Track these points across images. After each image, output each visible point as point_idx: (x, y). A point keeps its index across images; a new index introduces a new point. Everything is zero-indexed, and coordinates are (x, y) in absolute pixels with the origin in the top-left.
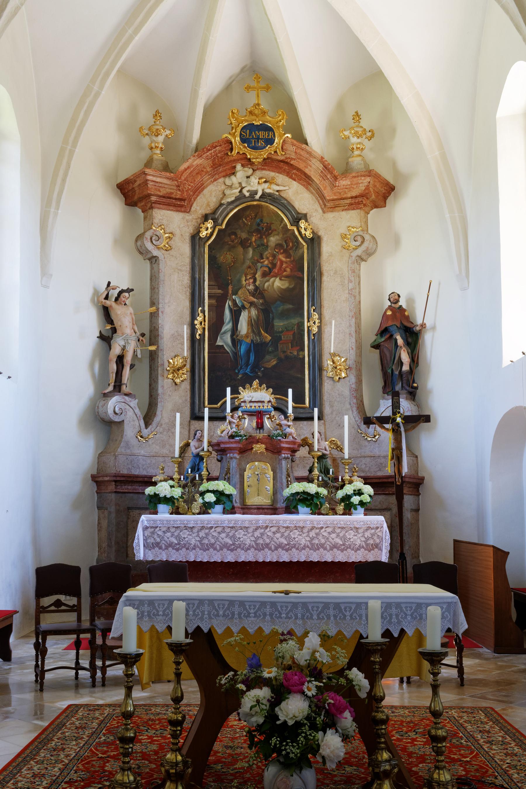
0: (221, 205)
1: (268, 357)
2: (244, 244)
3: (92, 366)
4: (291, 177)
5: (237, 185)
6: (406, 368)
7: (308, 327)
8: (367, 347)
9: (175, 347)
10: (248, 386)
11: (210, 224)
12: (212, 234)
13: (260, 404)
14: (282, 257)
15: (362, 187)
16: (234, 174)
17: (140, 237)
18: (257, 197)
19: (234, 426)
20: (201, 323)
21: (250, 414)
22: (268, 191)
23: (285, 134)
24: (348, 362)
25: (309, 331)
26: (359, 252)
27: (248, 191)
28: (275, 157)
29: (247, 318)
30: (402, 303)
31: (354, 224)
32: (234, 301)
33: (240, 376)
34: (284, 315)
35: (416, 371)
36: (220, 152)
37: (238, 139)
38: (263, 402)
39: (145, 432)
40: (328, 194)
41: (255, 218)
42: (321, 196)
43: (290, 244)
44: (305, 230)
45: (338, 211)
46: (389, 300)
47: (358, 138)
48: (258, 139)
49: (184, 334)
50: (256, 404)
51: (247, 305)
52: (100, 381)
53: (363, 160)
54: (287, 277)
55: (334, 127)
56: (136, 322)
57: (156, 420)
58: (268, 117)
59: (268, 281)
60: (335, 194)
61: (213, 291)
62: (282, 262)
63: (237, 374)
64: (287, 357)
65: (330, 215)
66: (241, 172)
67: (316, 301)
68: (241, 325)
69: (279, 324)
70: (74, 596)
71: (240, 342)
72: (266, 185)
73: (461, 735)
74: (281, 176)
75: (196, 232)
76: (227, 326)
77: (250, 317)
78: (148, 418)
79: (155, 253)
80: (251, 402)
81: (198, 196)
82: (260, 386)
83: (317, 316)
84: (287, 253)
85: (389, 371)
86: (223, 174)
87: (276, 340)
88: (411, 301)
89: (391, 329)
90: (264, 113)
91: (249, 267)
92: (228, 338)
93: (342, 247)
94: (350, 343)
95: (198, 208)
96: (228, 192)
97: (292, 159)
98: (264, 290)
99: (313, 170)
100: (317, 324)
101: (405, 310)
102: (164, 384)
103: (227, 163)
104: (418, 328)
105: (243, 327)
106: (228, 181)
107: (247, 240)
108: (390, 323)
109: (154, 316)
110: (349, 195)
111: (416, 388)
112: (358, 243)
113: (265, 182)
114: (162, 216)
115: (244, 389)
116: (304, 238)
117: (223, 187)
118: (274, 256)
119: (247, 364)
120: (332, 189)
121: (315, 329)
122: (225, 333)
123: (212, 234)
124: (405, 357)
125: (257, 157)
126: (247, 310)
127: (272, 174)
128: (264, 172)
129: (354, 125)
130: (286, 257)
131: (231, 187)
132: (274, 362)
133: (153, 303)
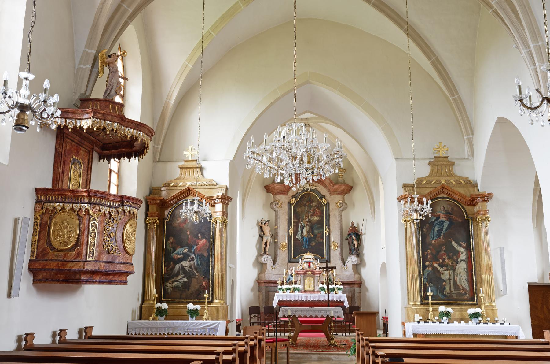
2: (305, 205)
3: (256, 246)
6: (356, 246)
8: (344, 239)
9: (283, 239)
17: (272, 204)
21: (307, 262)
26: (341, 209)
30: (355, 225)
34: (318, 228)
35: (360, 248)
39: (274, 267)
43: (320, 205)
49: (309, 326)
52: (259, 251)
56: (271, 231)
57: (277, 263)
65: (332, 196)
69: (316, 231)
76: (300, 232)
78: (274, 262)
79: (277, 209)
88: (358, 224)
92: (300, 236)
102: (279, 252)
105: (305, 232)
109: (276, 229)
114: (278, 197)
116: (324, 204)
121: (327, 234)
124: (356, 243)
133: (276, 225)
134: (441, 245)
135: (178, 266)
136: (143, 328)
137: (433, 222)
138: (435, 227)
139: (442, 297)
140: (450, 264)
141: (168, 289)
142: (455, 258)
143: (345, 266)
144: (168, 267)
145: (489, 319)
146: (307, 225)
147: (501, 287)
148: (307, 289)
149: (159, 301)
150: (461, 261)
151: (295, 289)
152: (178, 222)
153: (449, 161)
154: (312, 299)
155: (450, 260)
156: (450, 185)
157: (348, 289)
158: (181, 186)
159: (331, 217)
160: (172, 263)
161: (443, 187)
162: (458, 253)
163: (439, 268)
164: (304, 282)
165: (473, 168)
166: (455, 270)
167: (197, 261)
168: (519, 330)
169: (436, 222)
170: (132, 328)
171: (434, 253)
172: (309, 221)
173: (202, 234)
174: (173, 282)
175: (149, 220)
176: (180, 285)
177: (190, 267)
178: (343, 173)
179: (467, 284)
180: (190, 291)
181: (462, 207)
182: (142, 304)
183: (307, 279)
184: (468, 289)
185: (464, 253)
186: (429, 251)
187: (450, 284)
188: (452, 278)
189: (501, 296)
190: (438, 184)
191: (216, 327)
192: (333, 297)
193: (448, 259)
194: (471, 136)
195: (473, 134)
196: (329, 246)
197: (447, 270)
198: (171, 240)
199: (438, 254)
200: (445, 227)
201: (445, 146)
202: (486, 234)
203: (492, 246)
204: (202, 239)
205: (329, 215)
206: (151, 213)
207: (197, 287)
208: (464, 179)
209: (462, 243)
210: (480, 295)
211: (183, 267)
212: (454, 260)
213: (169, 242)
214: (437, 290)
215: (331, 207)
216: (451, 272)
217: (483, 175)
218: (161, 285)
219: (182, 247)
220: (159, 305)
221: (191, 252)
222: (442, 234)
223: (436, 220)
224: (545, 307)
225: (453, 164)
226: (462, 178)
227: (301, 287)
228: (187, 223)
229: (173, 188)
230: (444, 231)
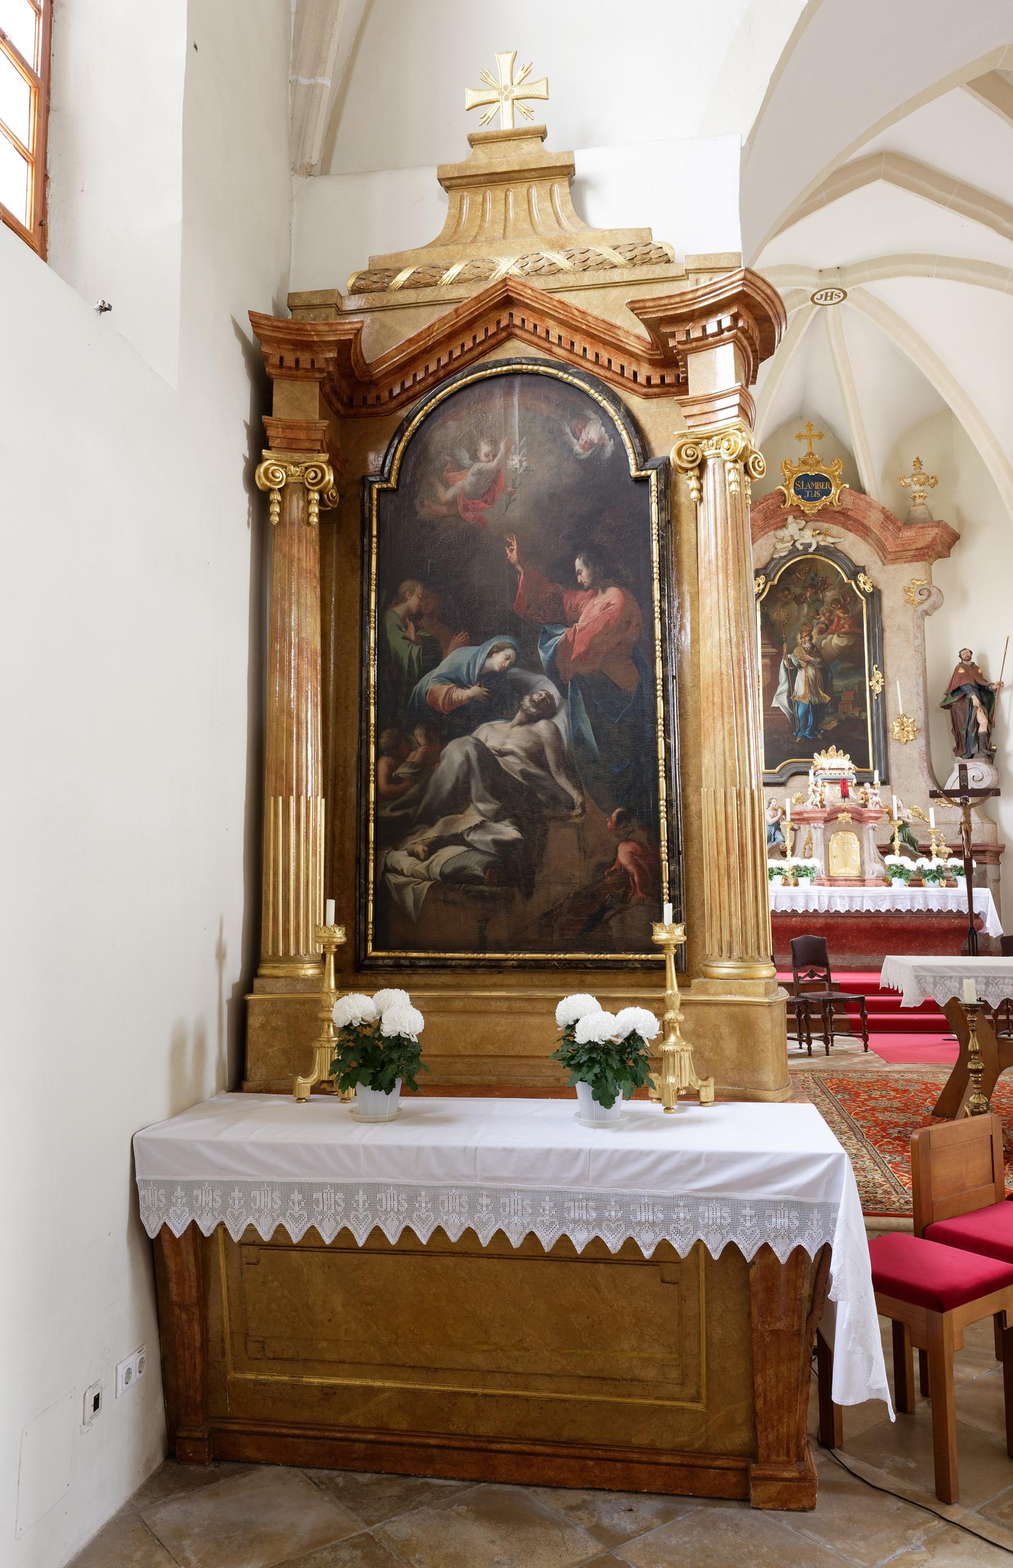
0: (772, 559)
1: (827, 719)
2: (799, 600)
4: (847, 528)
5: (789, 538)
6: (983, 729)
12: (764, 590)
15: (929, 538)
18: (811, 550)
21: (833, 781)
22: (822, 543)
24: (916, 724)
25: (871, 691)
26: (925, 606)
27: (802, 544)
29: (803, 678)
32: (789, 661)
34: (844, 674)
35: (994, 732)
36: (772, 504)
37: (792, 491)
40: (890, 545)
43: (848, 599)
44: (865, 583)
46: (960, 656)
48: (814, 489)
51: (803, 664)
53: (927, 509)
54: (845, 633)
55: (890, 474)
60: (897, 546)
61: (767, 650)
62: (839, 618)
63: (795, 737)
65: (891, 568)
66: (793, 527)
67: (879, 660)
69: (838, 684)
72: (820, 538)
73: (890, 1166)
76: (783, 687)
83: (881, 675)
84: (844, 608)
85: (964, 732)
87: (836, 701)
88: (982, 657)
89: (965, 688)
91: (805, 624)
93: (906, 601)
94: (918, 703)
96: (779, 546)
99: (873, 520)
101: (978, 668)
104: (994, 687)
106: (781, 533)
107: (801, 595)
108: (964, 682)
111: (995, 751)
112: (924, 597)
113: (819, 534)
116: (863, 592)
117: (774, 540)
118: (831, 612)
119: (806, 728)
120: (894, 540)
121: (878, 689)
122: (780, 694)
124: (982, 719)
127: (826, 525)
128: (817, 523)
129: (914, 472)
131: (782, 540)
135: (455, 754)
136: (247, 1187)
141: (400, 888)
144: (399, 759)
148: (836, 871)
149: (356, 971)
151: (800, 872)
152: (447, 495)
154: (868, 906)
158: (458, 281)
160: (419, 735)
164: (827, 848)
167: (573, 717)
170: (170, 1186)
172: (814, 650)
173: (596, 557)
174: (434, 847)
175: (276, 469)
176: (475, 864)
177: (535, 754)
178: (928, 489)
180: (539, 903)
182: (248, 983)
191: (811, 1187)
198: (413, 602)
204: (597, 586)
206: (289, 426)
207: (581, 875)
211: (488, 759)
213: (399, 610)
215: (888, 603)
218: (361, 864)
219: (476, 639)
220: (354, 1007)
221: (535, 666)
227: (815, 862)
228: (501, 498)
229: (411, 296)
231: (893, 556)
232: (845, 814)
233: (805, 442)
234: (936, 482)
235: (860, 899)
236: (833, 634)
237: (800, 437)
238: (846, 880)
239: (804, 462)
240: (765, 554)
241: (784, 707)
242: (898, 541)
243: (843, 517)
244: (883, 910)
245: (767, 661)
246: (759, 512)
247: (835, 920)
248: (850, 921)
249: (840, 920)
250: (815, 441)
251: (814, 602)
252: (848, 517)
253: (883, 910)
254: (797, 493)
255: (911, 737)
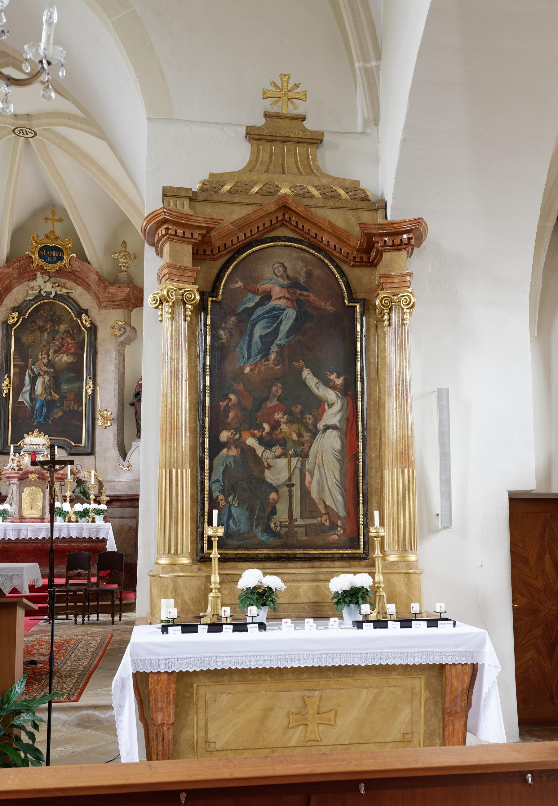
0: (25, 301)
1: (56, 410)
2: (42, 329)
4: (77, 283)
5: (38, 288)
7: (86, 390)
10: (30, 433)
11: (16, 315)
12: (17, 321)
13: (37, 447)
14: (68, 340)
16: (35, 279)
18: (52, 296)
19: (16, 462)
20: (7, 386)
22: (59, 293)
23: (71, 254)
26: (122, 339)
27: (45, 292)
28: (64, 269)
31: (119, 319)
32: (33, 370)
33: (35, 424)
34: (69, 381)
36: (24, 264)
37: (37, 255)
38: (39, 445)
41: (50, 311)
42: (97, 298)
43: (75, 331)
44: (86, 321)
45: (110, 309)
47: (124, 259)
48: (52, 256)
50: (34, 446)
51: (42, 373)
54: (72, 354)
55: (109, 250)
58: (59, 241)
59: (58, 356)
60: (106, 298)
62: (68, 343)
63: (33, 422)
64: (70, 410)
65: (104, 312)
68: (37, 387)
69: (65, 387)
70: (393, 603)
71: (36, 399)
72: (58, 289)
74: (70, 282)
75: (5, 320)
76: (27, 388)
77: (44, 382)
80: (31, 445)
81: (8, 294)
82: (40, 433)
84: (72, 337)
86: (27, 279)
87: (63, 398)
90: (57, 238)
91: (44, 346)
95: (8, 302)
97: (77, 271)
98: (55, 363)
99: (93, 278)
100: (91, 388)
103: (30, 272)
106: (32, 284)
107: (43, 326)
110: (116, 299)
113: (58, 286)
115: (28, 435)
116: (85, 327)
117: (27, 288)
118: (63, 339)
119: (41, 416)
121: (90, 392)
122: (25, 392)
123: (17, 321)
125: (52, 268)
126: (42, 377)
128: (58, 279)
129: (122, 249)
130: (72, 340)
131: (33, 288)
132: (60, 414)
134: (269, 383)
137: (250, 311)
138: (254, 325)
139: (264, 538)
140: (295, 437)
142: (309, 419)
143: (126, 463)
145: (391, 608)
146: (46, 372)
147: (436, 505)
148: (26, 512)
150: (327, 428)
153: (305, 130)
154: (30, 535)
155: (295, 426)
156: (306, 201)
157: (117, 511)
159: (99, 356)
161: (284, 207)
162: (319, 405)
163: (260, 449)
165: (376, 159)
166: (306, 456)
168: (482, 644)
169: (259, 311)
171: (249, 404)
172: (50, 364)
178: (130, 262)
179: (340, 498)
181: (338, 267)
183: (26, 492)
184: (342, 513)
185: (337, 407)
186: (232, 397)
187: (290, 496)
188: (296, 481)
189: (433, 531)
190: (270, 194)
192: (81, 529)
193: (289, 422)
194: (374, 63)
195: (379, 58)
196: (94, 420)
197: (284, 455)
199: (259, 409)
200: (285, 327)
201: (297, 86)
202: (402, 347)
203: (415, 387)
205: (95, 353)
208: (347, 184)
209: (333, 377)
210: (373, 532)
212: (306, 426)
214: (250, 518)
215: (101, 335)
216: (294, 461)
217: (402, 171)
222: (274, 348)
223: (257, 305)
224: (547, 556)
225: (316, 140)
226: (341, 182)
230: (281, 339)
231: (105, 304)
232: (33, 475)
233: (51, 223)
234: (135, 257)
235: (25, 531)
236: (64, 353)
237: (46, 220)
238: (31, 518)
239: (48, 237)
240: (20, 297)
241: (27, 401)
242: (106, 295)
243: (74, 276)
244: (40, 538)
245: (17, 370)
246: (14, 268)
247: (10, 545)
248: (19, 545)
249: (13, 545)
250: (57, 224)
251: (52, 331)
252: (77, 277)
253: (40, 538)
254: (41, 257)
255: (109, 424)
